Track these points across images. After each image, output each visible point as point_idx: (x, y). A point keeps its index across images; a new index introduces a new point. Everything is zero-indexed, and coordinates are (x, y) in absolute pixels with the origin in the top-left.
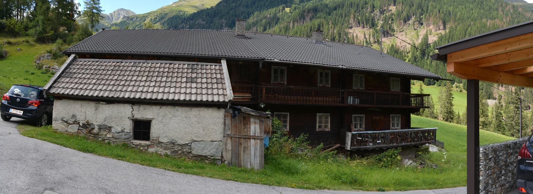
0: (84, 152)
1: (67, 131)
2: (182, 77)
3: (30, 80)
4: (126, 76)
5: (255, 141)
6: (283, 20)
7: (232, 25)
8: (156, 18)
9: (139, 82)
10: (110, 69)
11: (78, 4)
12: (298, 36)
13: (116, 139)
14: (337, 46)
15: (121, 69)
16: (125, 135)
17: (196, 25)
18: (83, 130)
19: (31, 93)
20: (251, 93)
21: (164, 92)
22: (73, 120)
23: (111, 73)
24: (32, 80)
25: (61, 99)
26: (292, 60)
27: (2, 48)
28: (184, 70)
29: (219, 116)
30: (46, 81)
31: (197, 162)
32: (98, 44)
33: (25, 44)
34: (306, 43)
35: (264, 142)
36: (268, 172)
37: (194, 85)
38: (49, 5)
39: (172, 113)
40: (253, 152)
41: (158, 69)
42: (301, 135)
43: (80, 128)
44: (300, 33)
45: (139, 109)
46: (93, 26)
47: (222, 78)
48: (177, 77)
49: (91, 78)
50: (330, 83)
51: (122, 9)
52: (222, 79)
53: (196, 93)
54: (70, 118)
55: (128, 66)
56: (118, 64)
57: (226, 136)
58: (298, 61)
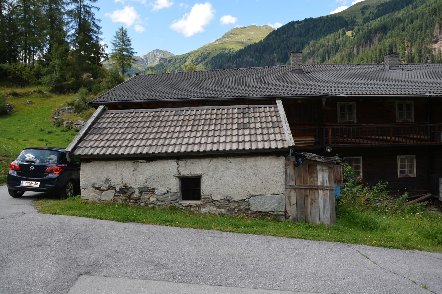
0: (124, 222)
1: (100, 200)
2: (232, 124)
3: (47, 141)
4: (167, 127)
5: (323, 192)
6: (345, 46)
7: (285, 60)
8: (198, 59)
9: (183, 133)
10: (148, 121)
11: (104, 45)
12: (365, 62)
13: (162, 202)
14: (419, 69)
15: (161, 119)
16: (172, 196)
17: (244, 62)
18: (121, 195)
19: (49, 158)
20: (314, 136)
21: (213, 143)
22: (107, 185)
23: (149, 125)
24: (50, 141)
25: (90, 162)
26: (362, 93)
27: (4, 101)
28: (234, 115)
29: (279, 165)
30: (68, 140)
31: (257, 220)
32: (132, 91)
33: (38, 95)
34: (378, 70)
35: (334, 192)
36: (341, 227)
37: (247, 132)
38: (68, 47)
39: (224, 165)
40: (321, 205)
41: (204, 116)
42: (378, 183)
43: (117, 194)
44: (367, 59)
45: (185, 164)
46: (124, 71)
47: (279, 121)
48: (227, 124)
49: (125, 133)
50: (413, 116)
51: (158, 51)
52: (278, 122)
53: (250, 141)
54: (103, 183)
55: (169, 116)
56: (157, 114)
57: (289, 187)
58: (369, 93)
